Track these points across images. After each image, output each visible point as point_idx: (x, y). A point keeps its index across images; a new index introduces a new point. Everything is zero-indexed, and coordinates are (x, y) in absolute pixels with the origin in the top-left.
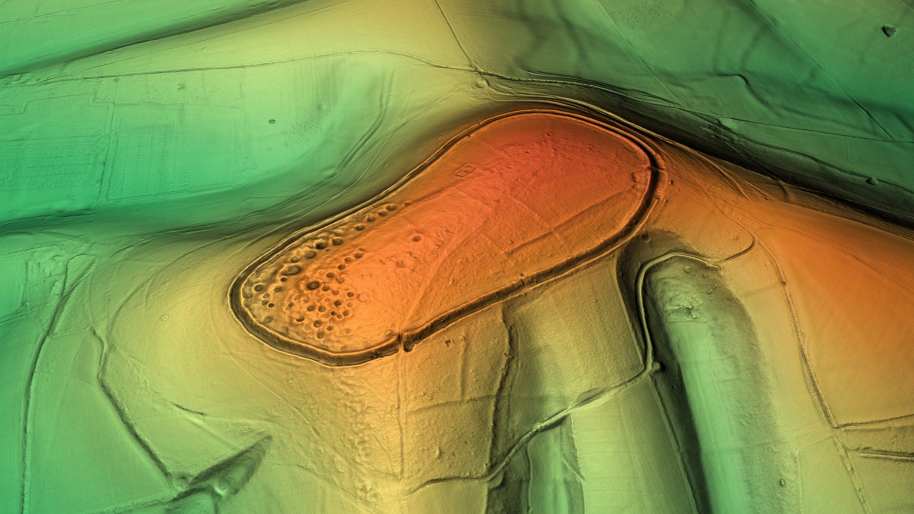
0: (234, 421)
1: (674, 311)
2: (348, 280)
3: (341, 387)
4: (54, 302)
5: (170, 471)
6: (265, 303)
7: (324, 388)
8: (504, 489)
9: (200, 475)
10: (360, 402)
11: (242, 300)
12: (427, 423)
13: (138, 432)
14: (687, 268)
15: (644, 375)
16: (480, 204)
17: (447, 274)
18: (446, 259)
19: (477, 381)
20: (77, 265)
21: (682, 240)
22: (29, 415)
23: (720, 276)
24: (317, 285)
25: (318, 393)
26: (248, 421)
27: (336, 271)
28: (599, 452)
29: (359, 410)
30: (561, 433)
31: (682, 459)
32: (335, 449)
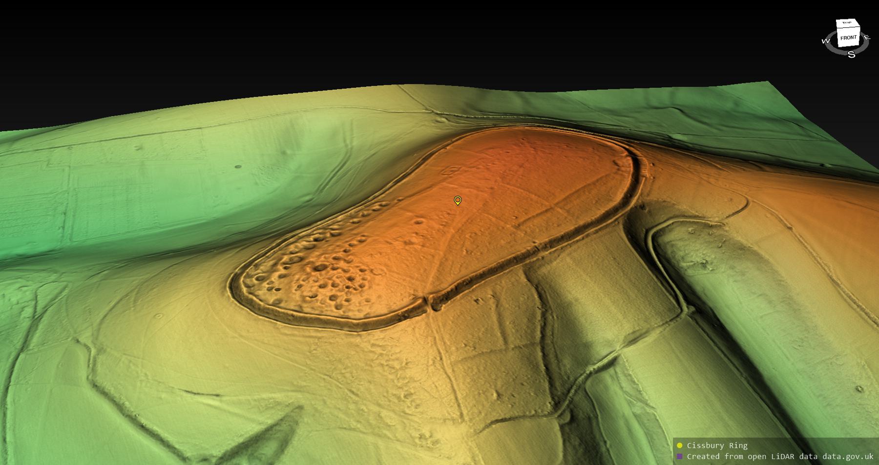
0: (256, 397)
1: (689, 267)
2: (356, 259)
4: (26, 324)
5: (188, 454)
6: (270, 289)
7: (353, 353)
8: (574, 425)
9: (225, 454)
10: (397, 359)
11: (245, 290)
12: (476, 370)
13: (143, 421)
14: (690, 229)
15: (683, 316)
16: (475, 192)
17: (459, 246)
18: (453, 236)
19: (517, 331)
20: (46, 293)
22: (8, 425)
24: (324, 267)
25: (348, 358)
26: (273, 395)
27: (341, 254)
28: (657, 391)
29: (398, 367)
30: (616, 372)
31: (748, 383)
32: (379, 405)
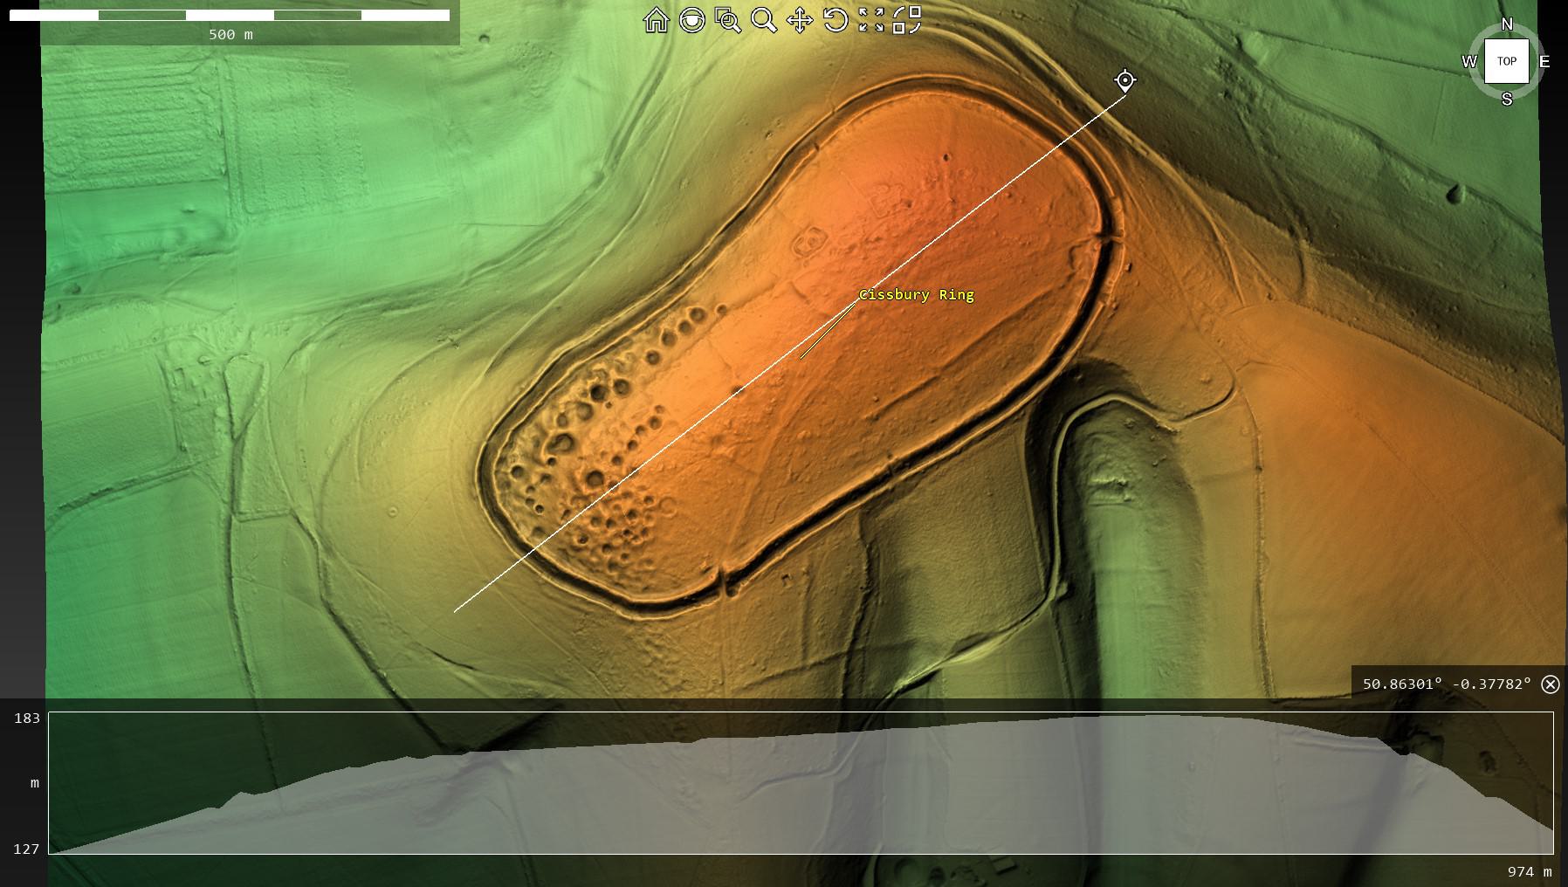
3: (648, 648)
21: (1130, 379)
23: (1174, 445)
26: (531, 683)
